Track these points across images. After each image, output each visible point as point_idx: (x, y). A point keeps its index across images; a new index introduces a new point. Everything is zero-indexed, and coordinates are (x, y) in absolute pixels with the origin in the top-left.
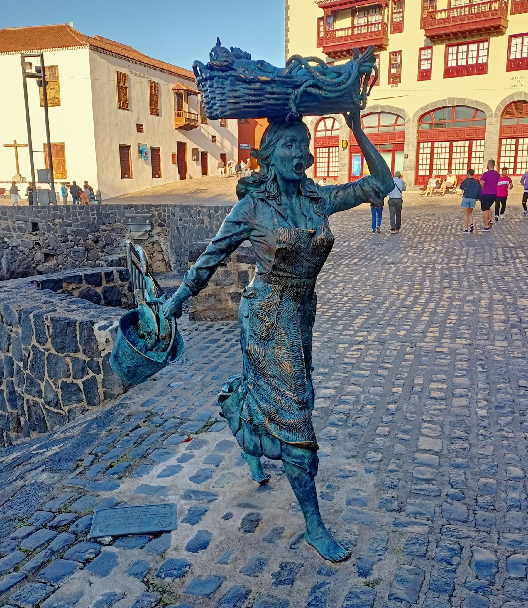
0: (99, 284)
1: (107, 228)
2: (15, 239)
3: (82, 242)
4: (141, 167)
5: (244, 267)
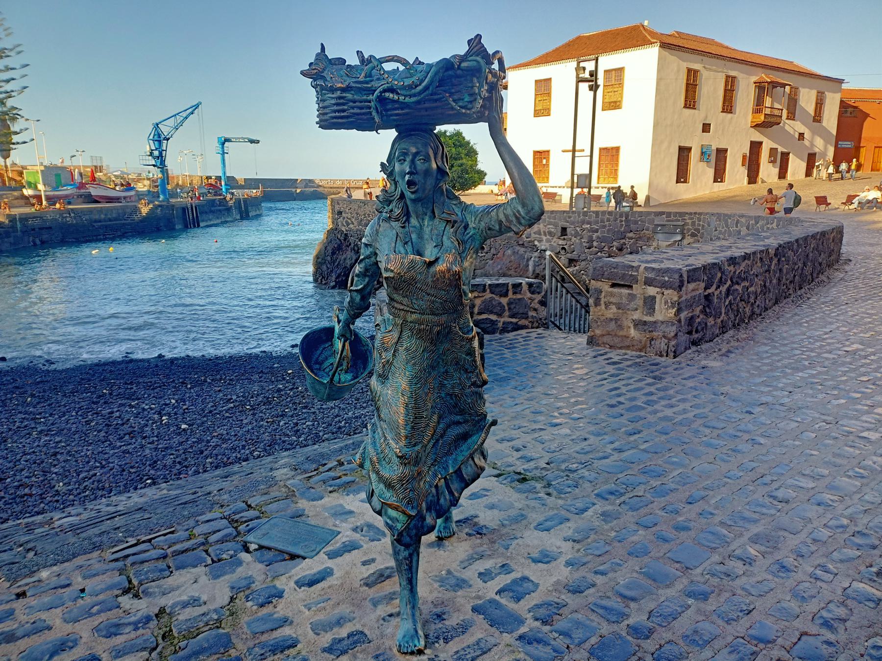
0: (506, 295)
1: (634, 236)
2: (544, 242)
3: (606, 249)
4: (701, 173)
5: (652, 291)
